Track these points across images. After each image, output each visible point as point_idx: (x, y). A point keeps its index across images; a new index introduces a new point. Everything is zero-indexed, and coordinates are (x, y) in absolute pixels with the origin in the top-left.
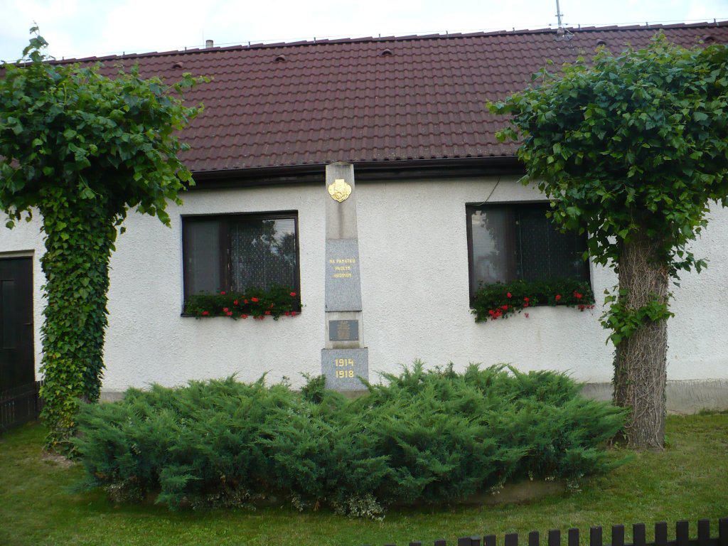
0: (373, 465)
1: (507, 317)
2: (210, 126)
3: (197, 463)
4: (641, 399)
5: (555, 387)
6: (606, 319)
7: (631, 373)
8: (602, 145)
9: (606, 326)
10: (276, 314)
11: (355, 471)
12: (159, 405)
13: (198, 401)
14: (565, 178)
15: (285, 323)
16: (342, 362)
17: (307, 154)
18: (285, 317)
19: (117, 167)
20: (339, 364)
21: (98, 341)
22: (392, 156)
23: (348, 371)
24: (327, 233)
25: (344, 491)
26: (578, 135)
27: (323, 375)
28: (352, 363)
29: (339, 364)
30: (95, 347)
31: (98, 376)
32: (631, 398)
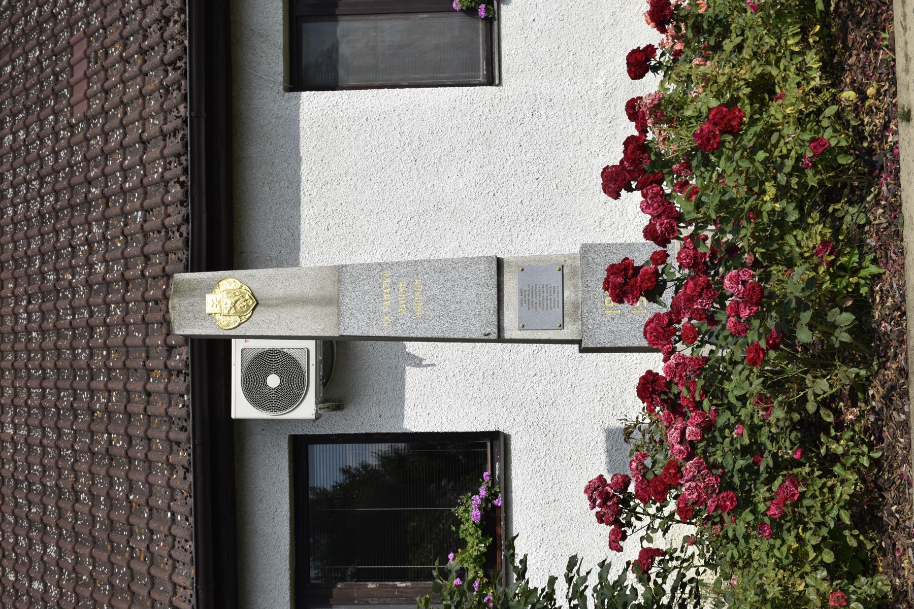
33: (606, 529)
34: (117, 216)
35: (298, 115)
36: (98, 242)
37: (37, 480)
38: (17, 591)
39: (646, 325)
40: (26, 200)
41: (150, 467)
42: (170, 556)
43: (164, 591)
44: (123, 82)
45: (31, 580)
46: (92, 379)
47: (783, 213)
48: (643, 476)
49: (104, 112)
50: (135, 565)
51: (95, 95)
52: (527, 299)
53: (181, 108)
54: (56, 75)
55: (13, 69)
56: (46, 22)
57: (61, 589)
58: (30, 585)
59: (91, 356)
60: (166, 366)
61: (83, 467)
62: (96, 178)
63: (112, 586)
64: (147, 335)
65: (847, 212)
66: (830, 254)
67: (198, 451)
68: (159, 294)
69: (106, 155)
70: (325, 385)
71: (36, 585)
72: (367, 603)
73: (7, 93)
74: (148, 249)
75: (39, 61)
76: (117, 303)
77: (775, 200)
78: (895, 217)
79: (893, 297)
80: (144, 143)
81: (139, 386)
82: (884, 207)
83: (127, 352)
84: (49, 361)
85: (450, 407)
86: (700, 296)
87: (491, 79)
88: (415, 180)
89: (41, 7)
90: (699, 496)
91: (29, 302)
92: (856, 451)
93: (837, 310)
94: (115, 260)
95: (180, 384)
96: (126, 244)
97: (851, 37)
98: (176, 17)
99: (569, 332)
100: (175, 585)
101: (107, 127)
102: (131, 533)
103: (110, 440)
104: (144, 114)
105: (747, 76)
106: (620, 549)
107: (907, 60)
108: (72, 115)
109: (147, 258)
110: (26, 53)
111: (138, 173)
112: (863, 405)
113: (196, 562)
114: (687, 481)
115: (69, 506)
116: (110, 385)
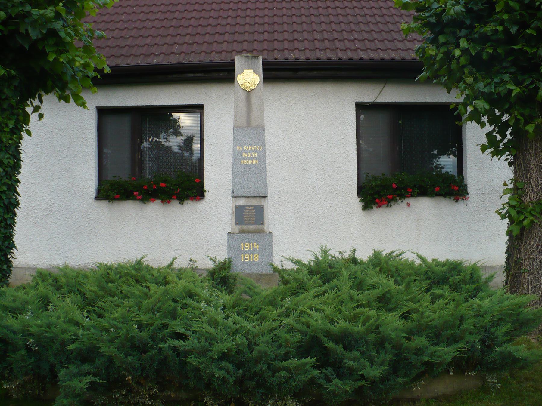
0: (297, 368)
1: (391, 206)
2: (126, 28)
3: (99, 362)
4: (535, 287)
5: (468, 277)
6: (504, 212)
7: (526, 262)
8: (510, 39)
9: (503, 217)
10: (182, 198)
11: (277, 374)
12: (65, 290)
13: (104, 288)
14: (471, 73)
15: (190, 206)
16: (247, 247)
17: (214, 53)
18: (190, 202)
19: (27, 47)
20: (245, 248)
21: (9, 222)
22: (292, 56)
23: (253, 255)
24: (235, 121)
25: (262, 393)
26: (488, 29)
27: (229, 259)
28: (257, 247)
29: (245, 248)
30: (5, 228)
31: (9, 256)
32: (525, 286)
85: (215, 175)
88: (316, 160)
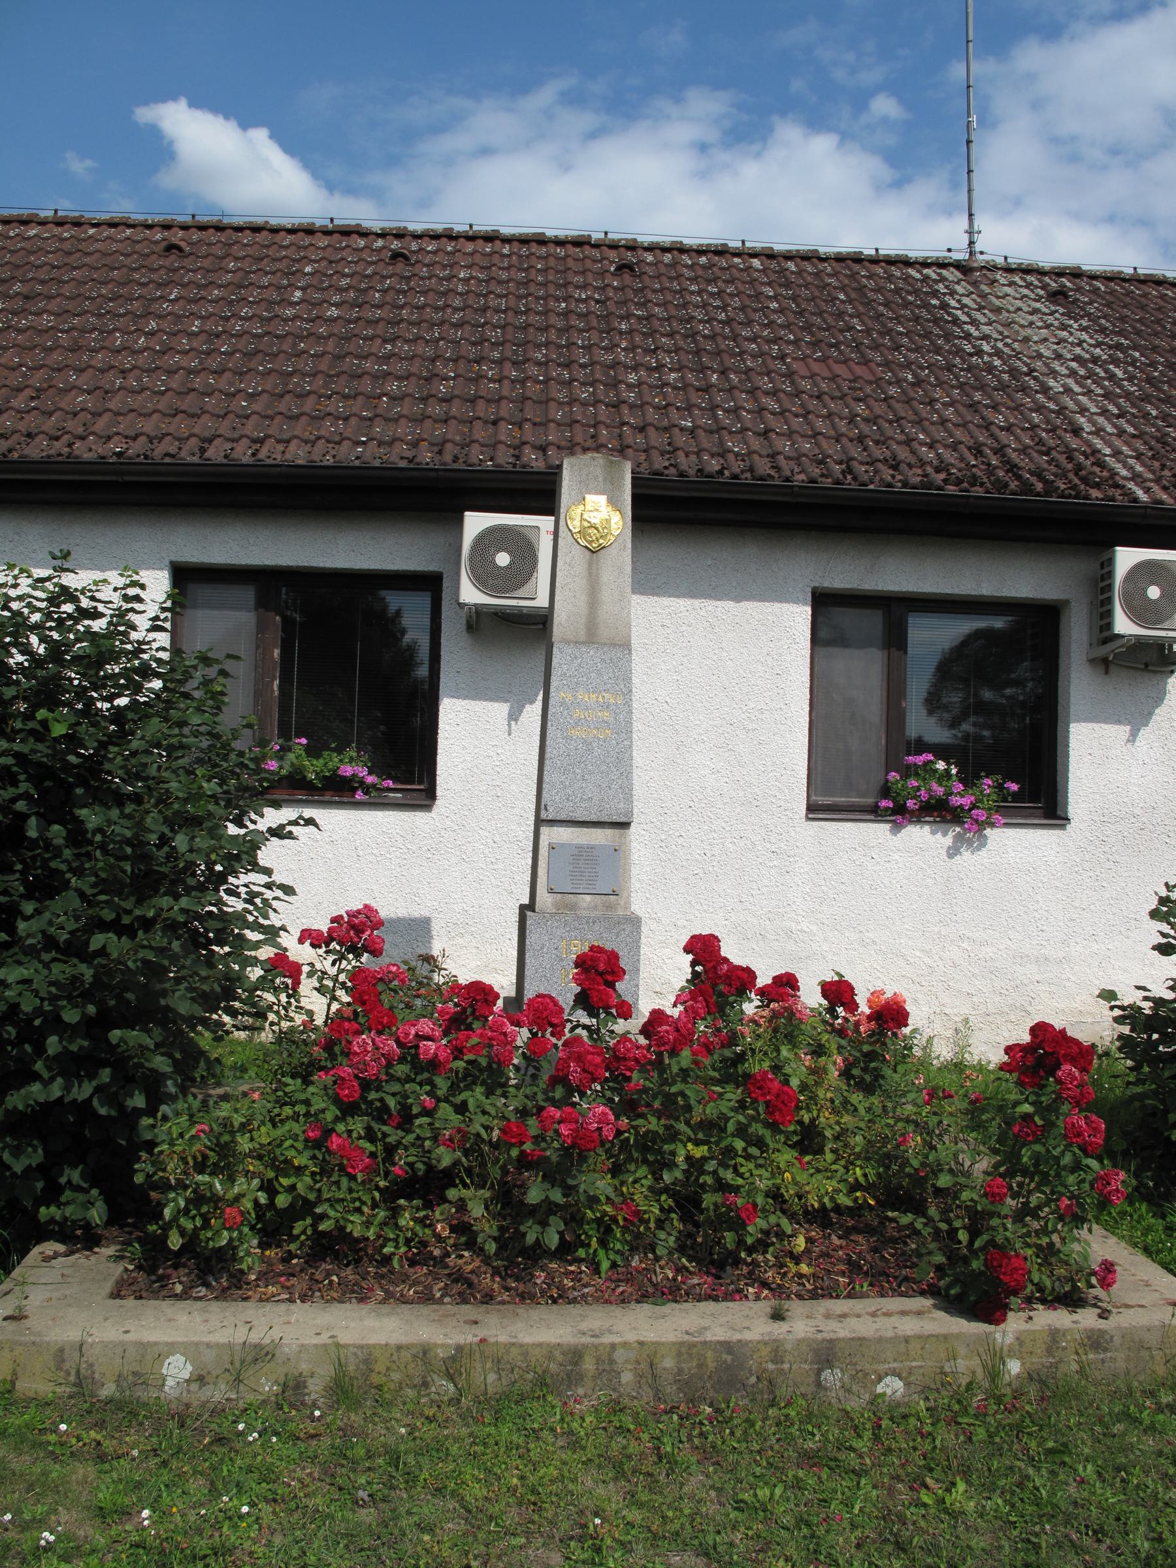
33: (324, 926)
34: (688, 400)
35: (787, 601)
36: (660, 378)
37: (409, 300)
38: (293, 274)
39: (550, 997)
40: (705, 305)
41: (416, 420)
42: (319, 438)
43: (281, 430)
44: (830, 415)
45: (303, 289)
46: (514, 363)
47: (672, 1165)
48: (381, 979)
49: (798, 393)
50: (312, 399)
51: (815, 384)
52: (583, 853)
53: (802, 477)
54: (836, 346)
55: (842, 302)
56: (891, 339)
57: (292, 320)
58: (298, 288)
59: (539, 364)
60: (524, 443)
61: (420, 348)
62: (728, 380)
63: (291, 374)
64: (559, 424)
65: (669, 1234)
66: (625, 1219)
67: (434, 474)
68: (602, 440)
69: (752, 392)
70: (496, 614)
71: (298, 294)
72: (258, 647)
73: (817, 294)
74: (651, 432)
75: (851, 328)
76: (594, 393)
77: (689, 1158)
78: (663, 1293)
79: (574, 1288)
80: (765, 433)
81: (503, 413)
82: (675, 1279)
83: (541, 402)
84: (534, 319)
86: (584, 1070)
87: (814, 810)
89: (907, 335)
90: (356, 1053)
91: (597, 302)
92: (401, 1240)
93: (562, 1227)
94: (640, 395)
95: (504, 458)
96: (658, 408)
97: (860, 1238)
98: (899, 477)
99: (543, 896)
100: (288, 441)
101: (782, 395)
102: (346, 397)
103: (447, 379)
104: (796, 437)
105: (822, 1119)
106: (301, 941)
107: (840, 1316)
108: (794, 359)
109: (642, 429)
110: (858, 316)
111: (733, 425)
112: (452, 1241)
113: (311, 467)
114: (373, 1041)
115: (379, 332)
116: (506, 382)
